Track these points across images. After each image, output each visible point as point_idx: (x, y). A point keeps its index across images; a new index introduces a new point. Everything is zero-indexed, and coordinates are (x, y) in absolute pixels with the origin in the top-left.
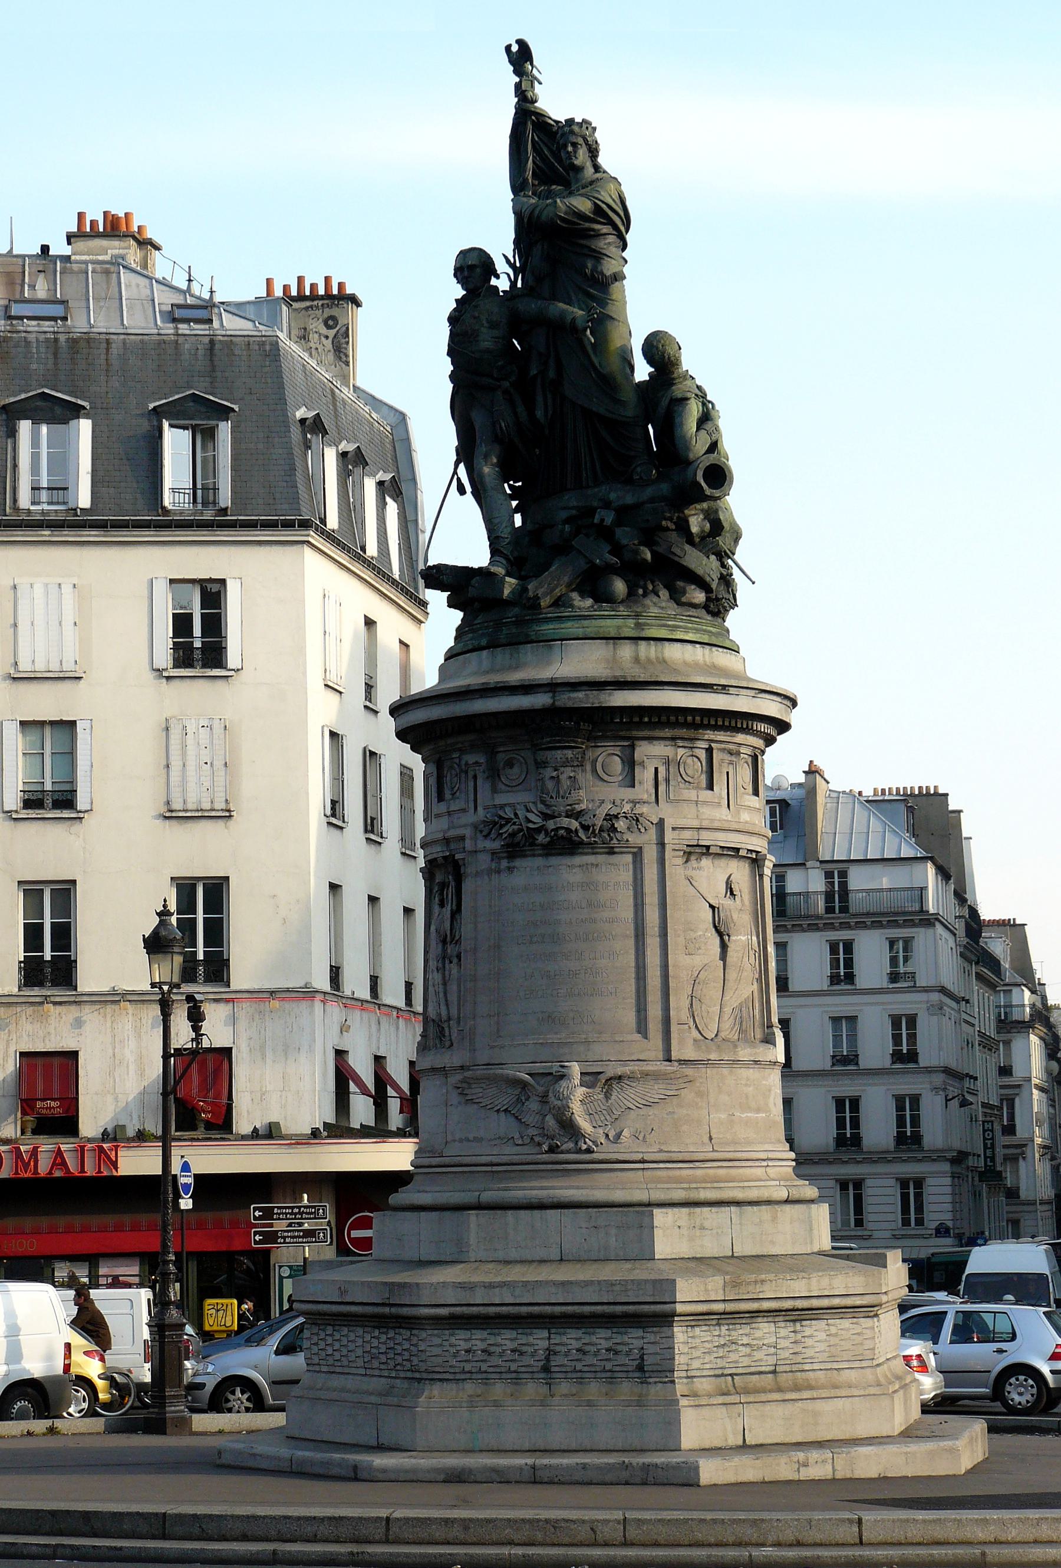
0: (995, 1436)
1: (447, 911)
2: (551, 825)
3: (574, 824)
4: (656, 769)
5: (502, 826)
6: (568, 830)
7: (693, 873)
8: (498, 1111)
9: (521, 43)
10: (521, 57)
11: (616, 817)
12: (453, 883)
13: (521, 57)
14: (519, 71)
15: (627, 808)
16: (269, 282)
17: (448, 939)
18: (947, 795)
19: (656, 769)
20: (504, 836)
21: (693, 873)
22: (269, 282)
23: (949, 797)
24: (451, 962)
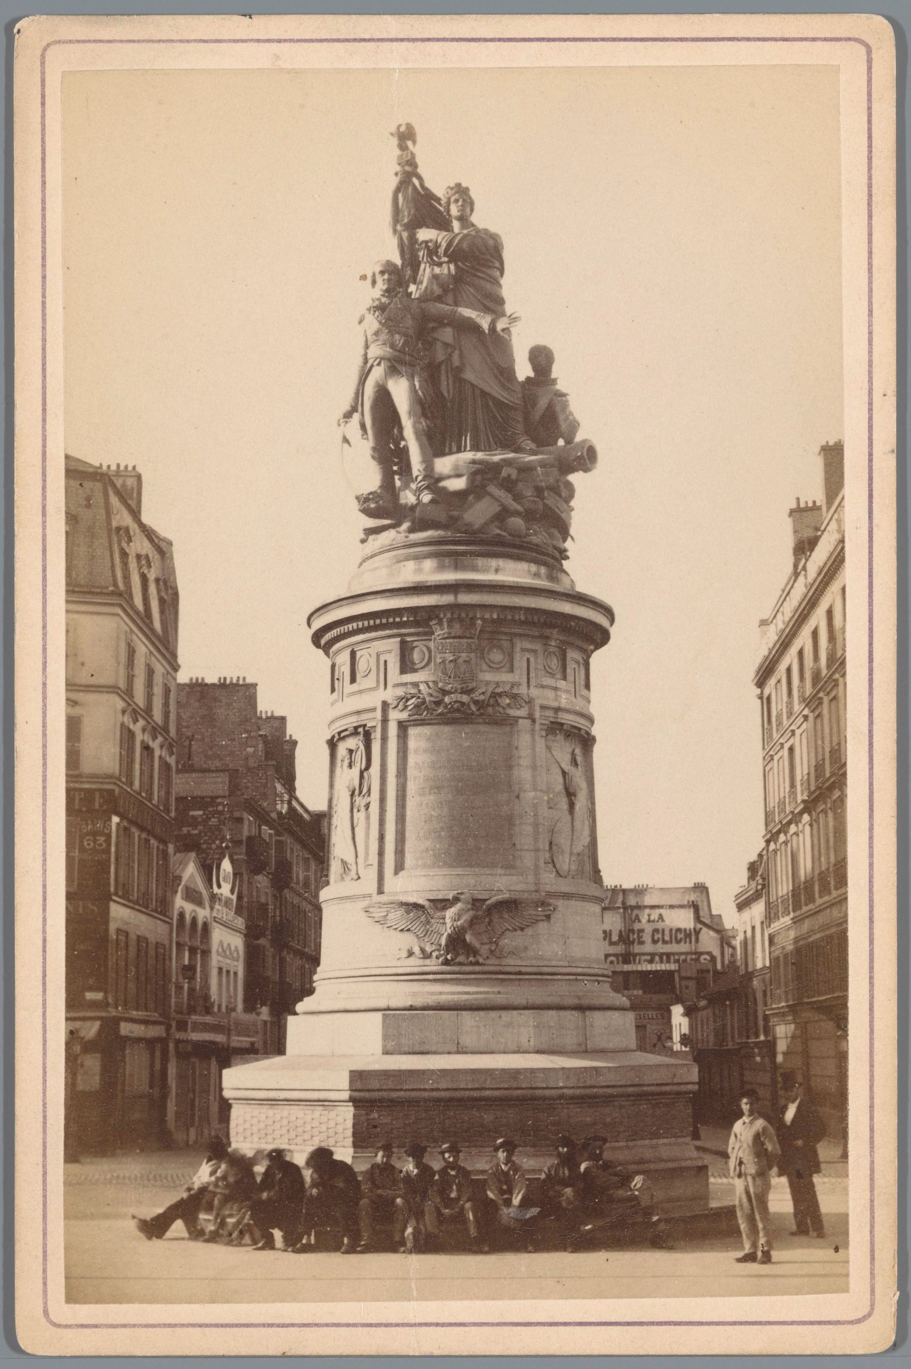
0: (842, 1211)
1: (356, 772)
2: (447, 700)
3: (465, 698)
4: (528, 660)
5: (408, 700)
6: (463, 704)
7: (550, 744)
8: (402, 930)
9: (409, 127)
10: (406, 136)
11: (500, 695)
12: (362, 747)
13: (406, 136)
14: (403, 147)
15: (507, 688)
16: (798, 499)
17: (357, 792)
18: (256, 685)
19: (528, 660)
20: (410, 708)
21: (550, 744)
22: (798, 499)
23: (258, 688)
24: (358, 811)
